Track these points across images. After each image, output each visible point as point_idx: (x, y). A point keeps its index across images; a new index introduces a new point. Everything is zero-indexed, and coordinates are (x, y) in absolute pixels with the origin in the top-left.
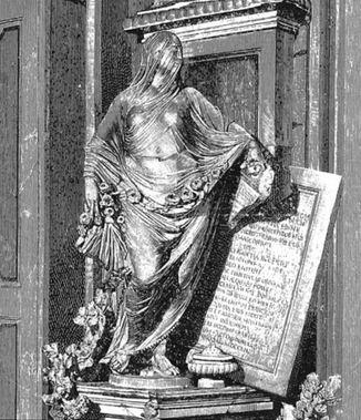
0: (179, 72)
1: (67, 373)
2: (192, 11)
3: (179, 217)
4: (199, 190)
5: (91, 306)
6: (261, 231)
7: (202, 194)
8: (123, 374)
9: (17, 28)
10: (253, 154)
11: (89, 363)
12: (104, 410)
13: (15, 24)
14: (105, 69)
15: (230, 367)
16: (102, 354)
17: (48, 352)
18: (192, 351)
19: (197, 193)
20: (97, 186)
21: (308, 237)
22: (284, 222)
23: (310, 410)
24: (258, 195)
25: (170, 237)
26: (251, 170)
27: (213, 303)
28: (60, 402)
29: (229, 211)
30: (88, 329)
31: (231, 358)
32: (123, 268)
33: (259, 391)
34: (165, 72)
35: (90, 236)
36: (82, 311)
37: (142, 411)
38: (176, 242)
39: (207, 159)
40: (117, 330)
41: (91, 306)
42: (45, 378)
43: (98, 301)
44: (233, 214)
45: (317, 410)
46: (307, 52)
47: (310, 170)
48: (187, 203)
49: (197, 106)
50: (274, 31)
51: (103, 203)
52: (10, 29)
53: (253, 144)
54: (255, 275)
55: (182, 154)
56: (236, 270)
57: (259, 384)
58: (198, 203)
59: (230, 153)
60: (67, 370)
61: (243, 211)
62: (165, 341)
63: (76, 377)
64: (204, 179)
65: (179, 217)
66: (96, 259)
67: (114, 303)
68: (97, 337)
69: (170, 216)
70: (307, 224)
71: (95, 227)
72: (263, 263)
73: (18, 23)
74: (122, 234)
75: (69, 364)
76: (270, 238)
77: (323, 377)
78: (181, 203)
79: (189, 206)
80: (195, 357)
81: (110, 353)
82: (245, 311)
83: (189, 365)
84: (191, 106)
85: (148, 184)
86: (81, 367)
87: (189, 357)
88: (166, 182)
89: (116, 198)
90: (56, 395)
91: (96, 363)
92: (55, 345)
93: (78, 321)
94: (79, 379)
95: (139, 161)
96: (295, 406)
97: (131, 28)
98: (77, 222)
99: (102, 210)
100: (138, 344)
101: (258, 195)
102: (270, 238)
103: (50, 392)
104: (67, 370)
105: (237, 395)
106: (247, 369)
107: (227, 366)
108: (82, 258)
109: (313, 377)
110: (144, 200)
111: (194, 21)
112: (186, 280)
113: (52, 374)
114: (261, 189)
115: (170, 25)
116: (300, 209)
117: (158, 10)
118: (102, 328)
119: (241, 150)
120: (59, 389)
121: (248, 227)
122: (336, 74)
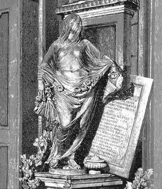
0: (80, 33)
1: (30, 168)
2: (86, 5)
3: (80, 98)
4: (89, 85)
5: (41, 138)
6: (117, 104)
7: (91, 87)
8: (55, 168)
9: (8, 12)
10: (114, 69)
11: (40, 163)
12: (47, 184)
13: (7, 11)
14: (47, 31)
15: (103, 165)
16: (46, 159)
17: (22, 159)
18: (86, 158)
19: (89, 87)
20: (44, 84)
21: (138, 107)
22: (127, 100)
23: (139, 184)
24: (116, 88)
25: (76, 107)
26: (113, 76)
27: (96, 136)
28: (27, 181)
29: (103, 95)
30: (40, 148)
31: (104, 161)
32: (55, 121)
33: (116, 176)
34: (74, 32)
35: (41, 106)
36: (37, 140)
37: (64, 185)
38: (79, 109)
39: (93, 71)
40: (52, 149)
41: (41, 138)
42: (20, 170)
43: (44, 135)
44: (105, 96)
45: (142, 184)
46: (138, 23)
47: (139, 77)
48: (84, 91)
49: (88, 48)
50: (123, 14)
51: (46, 91)
53: (114, 65)
54: (115, 124)
55: (82, 70)
56: (106, 121)
57: (116, 173)
58: (89, 91)
59: (103, 69)
60: (30, 166)
61: (109, 95)
62: (74, 153)
63: (34, 170)
64: (92, 80)
65: (80, 98)
66: (43, 116)
67: (51, 137)
68: (44, 152)
69: (76, 97)
70: (138, 101)
71: (42, 102)
72: (118, 118)
74: (55, 105)
75: (31, 164)
76: (121, 107)
77: (145, 170)
78: (81, 91)
79: (85, 93)
80: (88, 161)
81: (49, 159)
82: (110, 140)
83: (85, 164)
84: (86, 48)
85: (66, 83)
86: (36, 165)
87: (85, 161)
88: (75, 82)
89: (52, 89)
90: (25, 178)
91: (43, 163)
92: (25, 155)
93: (35, 144)
94: (36, 170)
95: (62, 72)
96: (132, 183)
97: (59, 13)
98: (35, 100)
99: (46, 94)
100: (62, 155)
101: (116, 88)
102: (121, 107)
103: (23, 176)
104: (30, 166)
105: (106, 178)
106: (111, 166)
107: (102, 165)
108: (37, 116)
109: (140, 169)
110: (65, 90)
111: (87, 10)
112: (83, 126)
113: (23, 168)
114: (117, 85)
115: (77, 11)
116: (134, 94)
117: (71, 5)
118: (46, 148)
119: (108, 68)
120: (27, 175)
121: (111, 102)
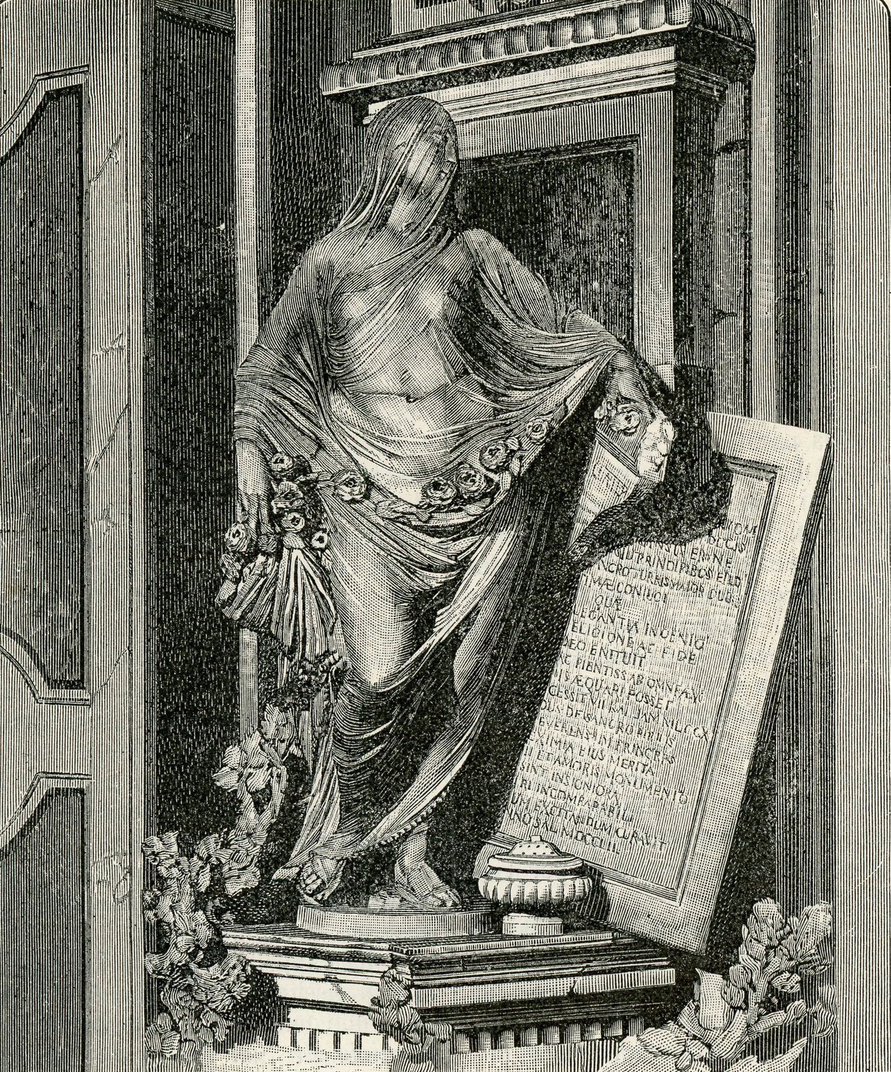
0: (450, 196)
1: (199, 902)
2: (478, 49)
3: (460, 531)
4: (498, 470)
5: (253, 743)
6: (644, 564)
7: (505, 480)
8: (325, 904)
9: (76, 91)
10: (624, 384)
11: (251, 879)
12: (287, 988)
13: (72, 81)
14: (278, 160)
15: (578, 886)
16: (281, 859)
17: (156, 855)
18: (487, 849)
19: (496, 477)
20: (267, 462)
21: (752, 580)
22: (697, 543)
23: (762, 985)
24: (636, 480)
25: (435, 580)
26: (621, 423)
27: (534, 736)
28: (186, 971)
29: (569, 526)
30: (248, 799)
31: (578, 864)
32: (327, 653)
33: (642, 942)
34: (416, 191)
35: (250, 580)
36: (233, 755)
37: (374, 992)
38: (448, 592)
39: (517, 396)
40: (313, 802)
41: (253, 743)
42: (150, 914)
43: (271, 730)
44: (579, 527)
45: (776, 983)
46: (746, 144)
47: (749, 424)
48: (471, 500)
49: (493, 273)
50: (669, 94)
51: (278, 504)
52: (66, 792)
53: (623, 361)
54: (631, 670)
55: (461, 385)
56: (586, 656)
57: (643, 927)
58: (499, 498)
59: (573, 381)
60: (199, 894)
61: (600, 518)
62: (424, 827)
63: (219, 913)
64: (513, 444)
65: (460, 531)
66: (266, 636)
67: (308, 736)
68: (267, 817)
69: (435, 532)
70: (751, 548)
71: (261, 559)
72: (647, 639)
73: (85, 784)
74: (325, 574)
75: (205, 882)
76: (663, 582)
77: (791, 909)
78: (460, 501)
79: (474, 509)
80: (494, 863)
81: (297, 855)
82: (607, 753)
83: (481, 883)
84: (477, 273)
85: (382, 457)
86: (233, 888)
87: (482, 862)
88: (424, 453)
89: (310, 488)
90: (175, 956)
91: (266, 876)
92: (172, 837)
93: (226, 779)
94: (228, 916)
95: (359, 400)
96: (726, 976)
97: (337, 90)
98: (222, 546)
99: (275, 518)
100: (363, 832)
101: (636, 480)
102: (663, 582)
103: (162, 949)
104: (199, 894)
105: (598, 952)
106: (614, 891)
107: (568, 884)
108: (231, 629)
109: (767, 908)
110: (374, 494)
111: (485, 73)
112: (472, 678)
113: (165, 903)
114: (644, 466)
115: (427, 83)
116: (733, 512)
117: (400, 47)
118: (278, 798)
119: (595, 374)
120: (182, 941)
121: (613, 557)
122: (816, 14)
